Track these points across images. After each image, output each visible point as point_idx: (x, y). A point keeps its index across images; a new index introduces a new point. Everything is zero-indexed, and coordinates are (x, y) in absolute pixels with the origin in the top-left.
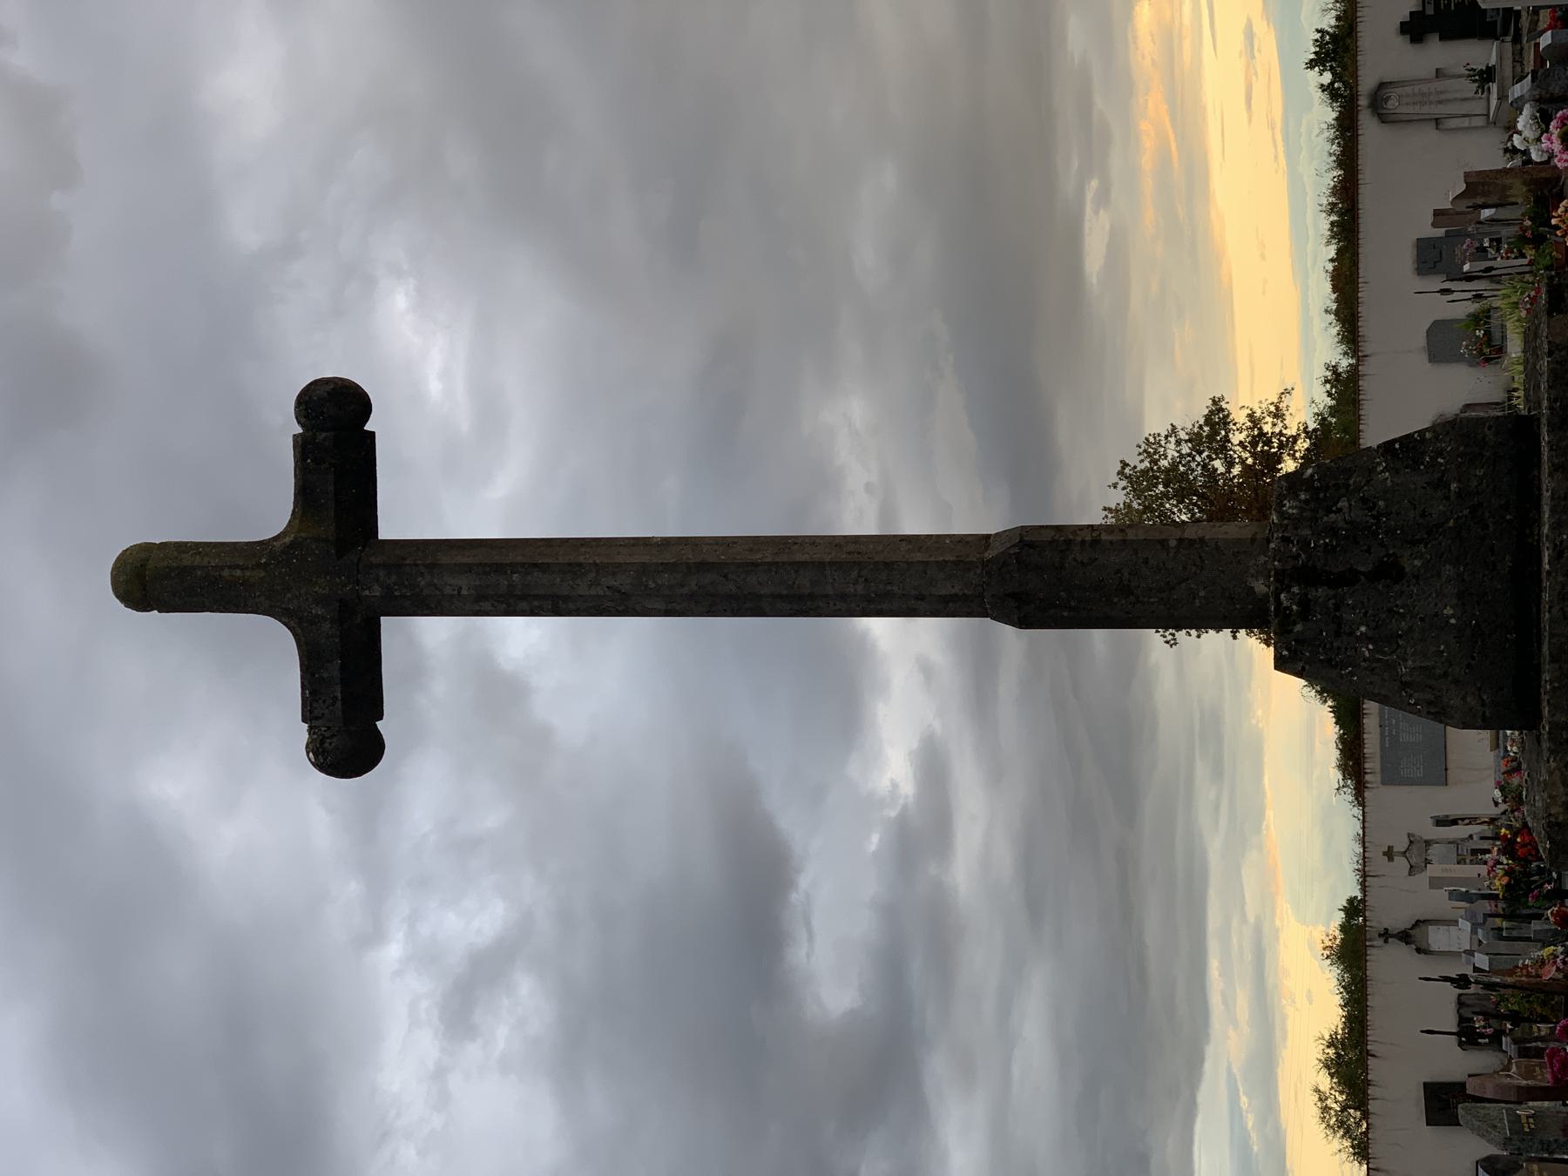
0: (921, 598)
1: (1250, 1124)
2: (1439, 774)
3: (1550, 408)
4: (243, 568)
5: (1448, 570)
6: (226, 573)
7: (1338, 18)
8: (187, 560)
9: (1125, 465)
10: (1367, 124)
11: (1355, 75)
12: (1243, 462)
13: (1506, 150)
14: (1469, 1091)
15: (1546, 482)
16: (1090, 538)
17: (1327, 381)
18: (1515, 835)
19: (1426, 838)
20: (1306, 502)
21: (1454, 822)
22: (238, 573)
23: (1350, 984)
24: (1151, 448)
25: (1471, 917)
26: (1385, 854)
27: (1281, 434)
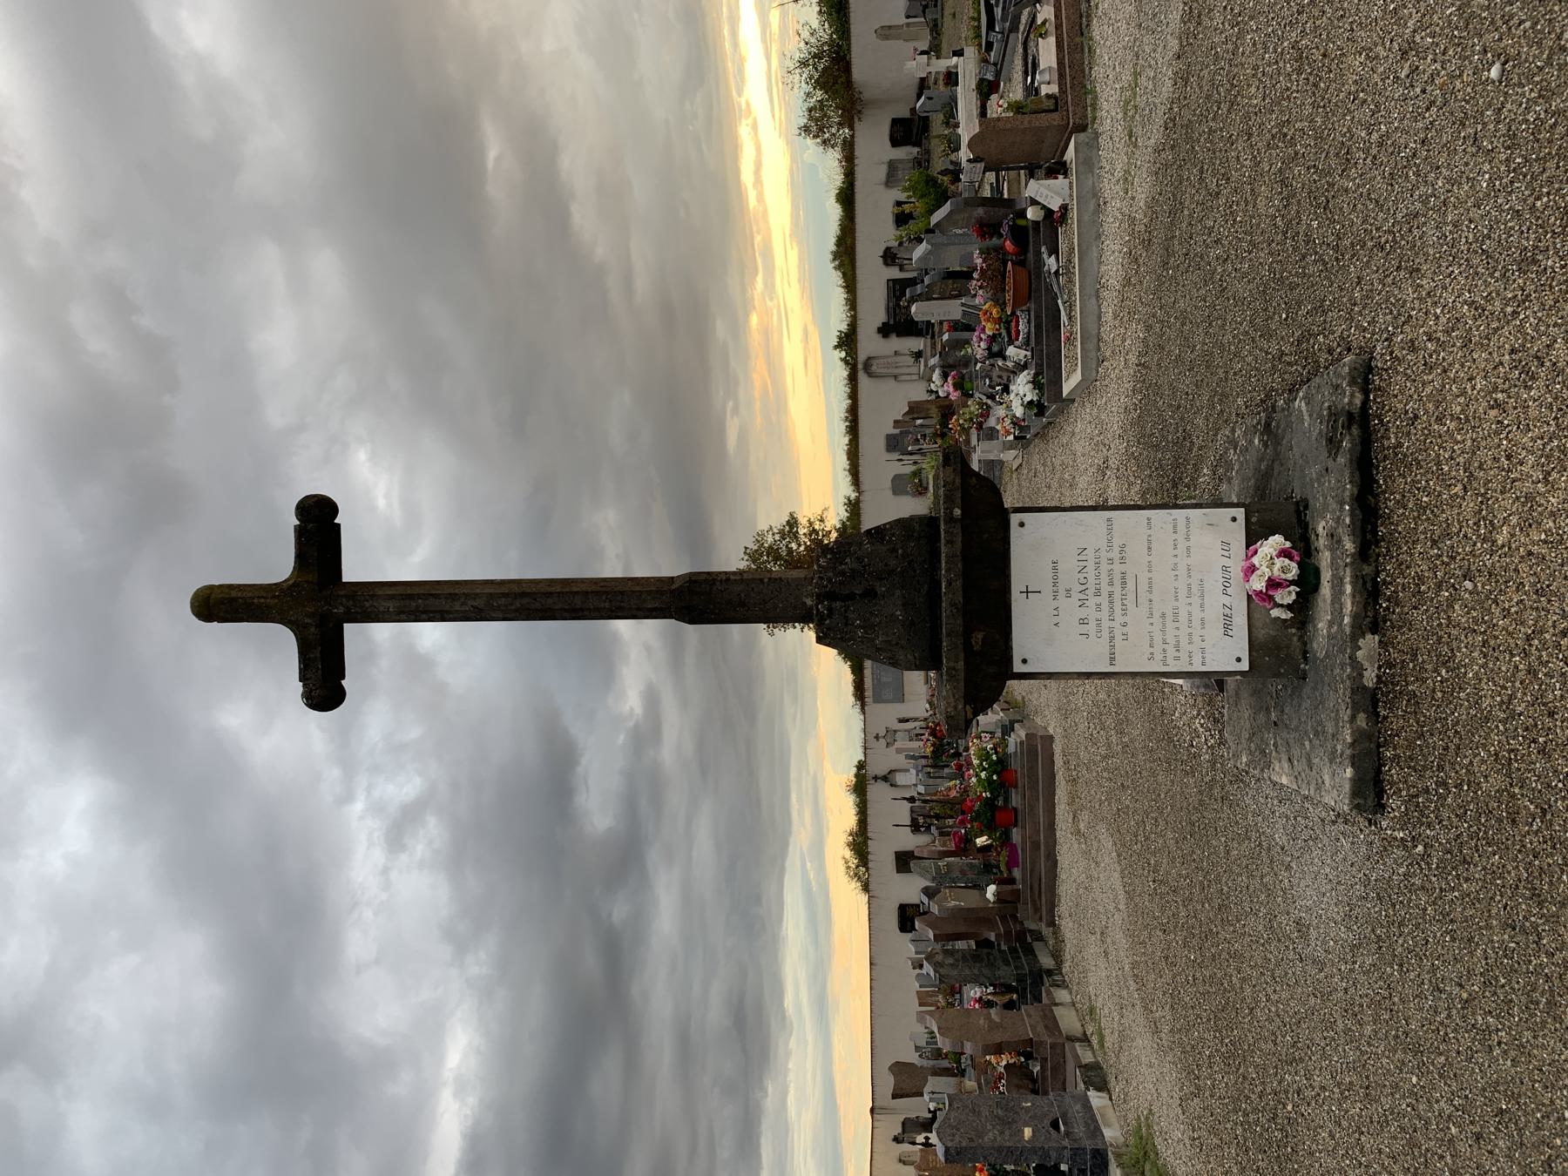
0: (638, 609)
1: (812, 876)
2: (900, 697)
3: (944, 512)
4: (265, 598)
5: (898, 592)
6: (256, 601)
7: (848, 325)
8: (234, 594)
9: (746, 548)
10: (862, 378)
11: (856, 353)
12: (805, 543)
13: (928, 391)
14: (916, 854)
15: (943, 548)
16: (727, 578)
17: (845, 504)
18: (936, 726)
19: (894, 728)
20: (830, 559)
21: (907, 721)
22: (263, 600)
23: (859, 804)
24: (761, 535)
25: (916, 767)
26: (875, 737)
27: (823, 529)
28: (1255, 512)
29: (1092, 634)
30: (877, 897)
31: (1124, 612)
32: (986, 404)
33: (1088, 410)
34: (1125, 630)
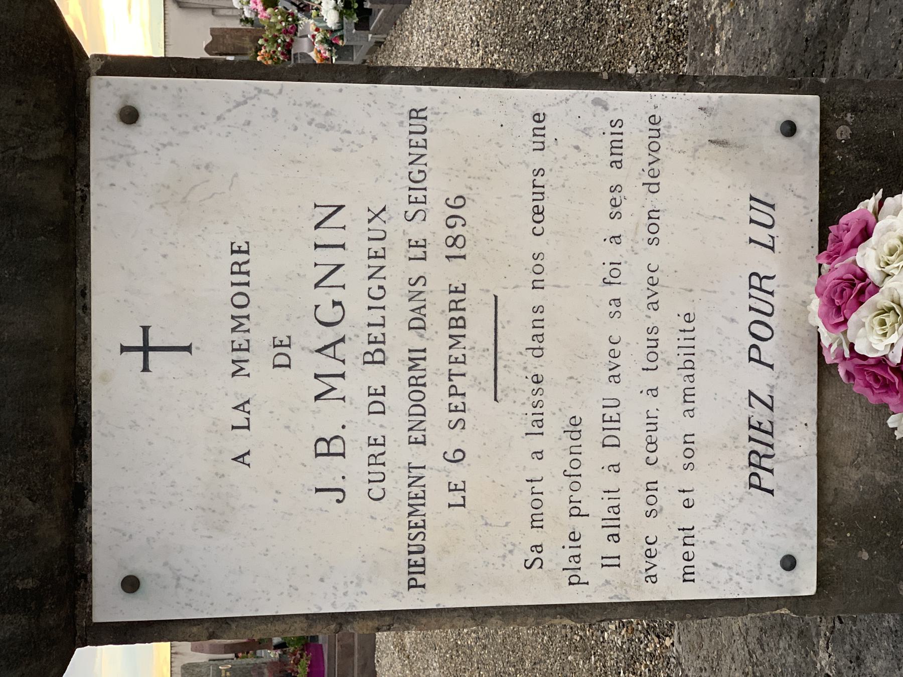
28: (845, 109)
29: (356, 489)
30: (181, 654)
31: (455, 416)
32: (292, 14)
33: (427, 11)
34: (458, 473)
